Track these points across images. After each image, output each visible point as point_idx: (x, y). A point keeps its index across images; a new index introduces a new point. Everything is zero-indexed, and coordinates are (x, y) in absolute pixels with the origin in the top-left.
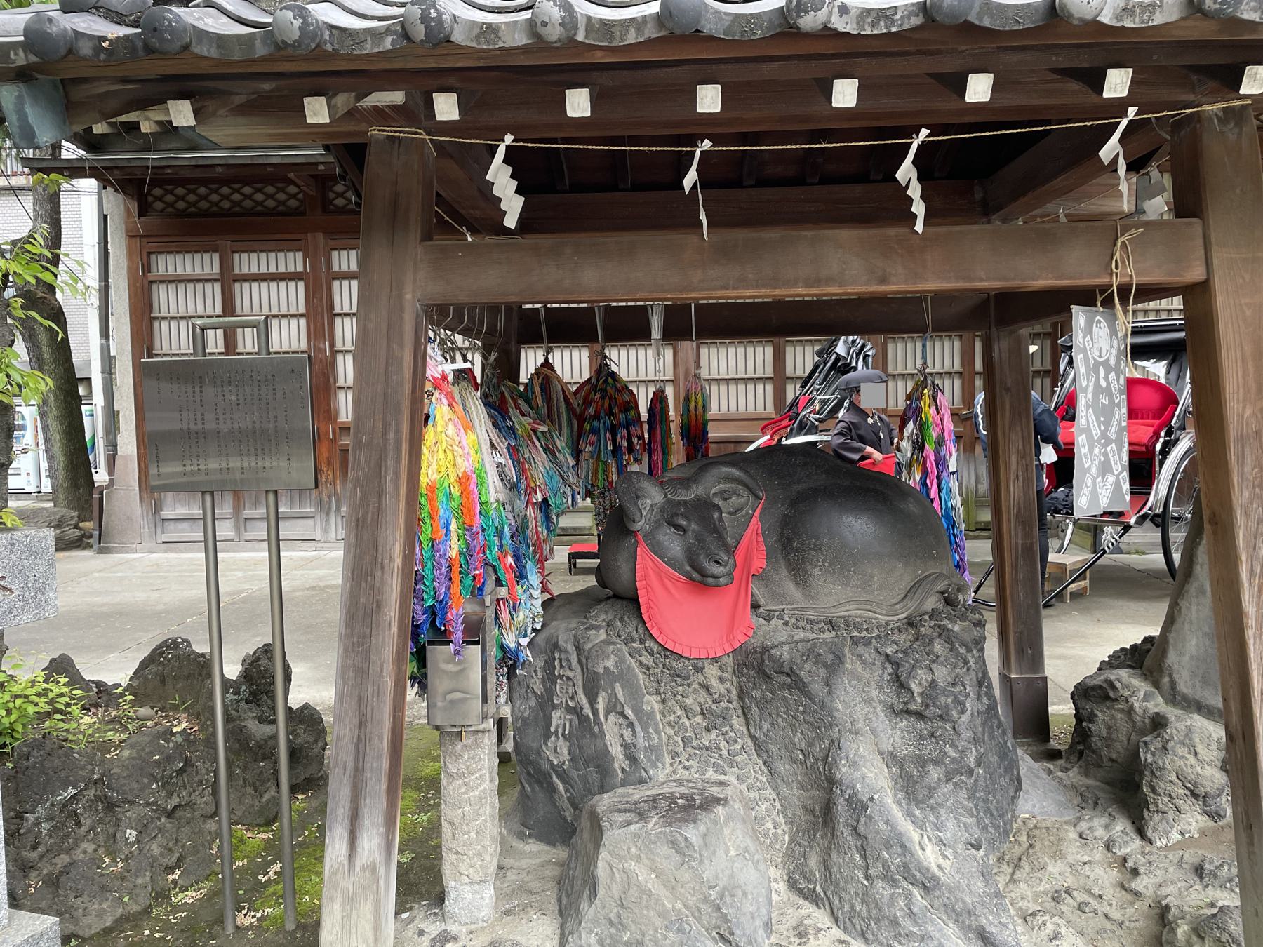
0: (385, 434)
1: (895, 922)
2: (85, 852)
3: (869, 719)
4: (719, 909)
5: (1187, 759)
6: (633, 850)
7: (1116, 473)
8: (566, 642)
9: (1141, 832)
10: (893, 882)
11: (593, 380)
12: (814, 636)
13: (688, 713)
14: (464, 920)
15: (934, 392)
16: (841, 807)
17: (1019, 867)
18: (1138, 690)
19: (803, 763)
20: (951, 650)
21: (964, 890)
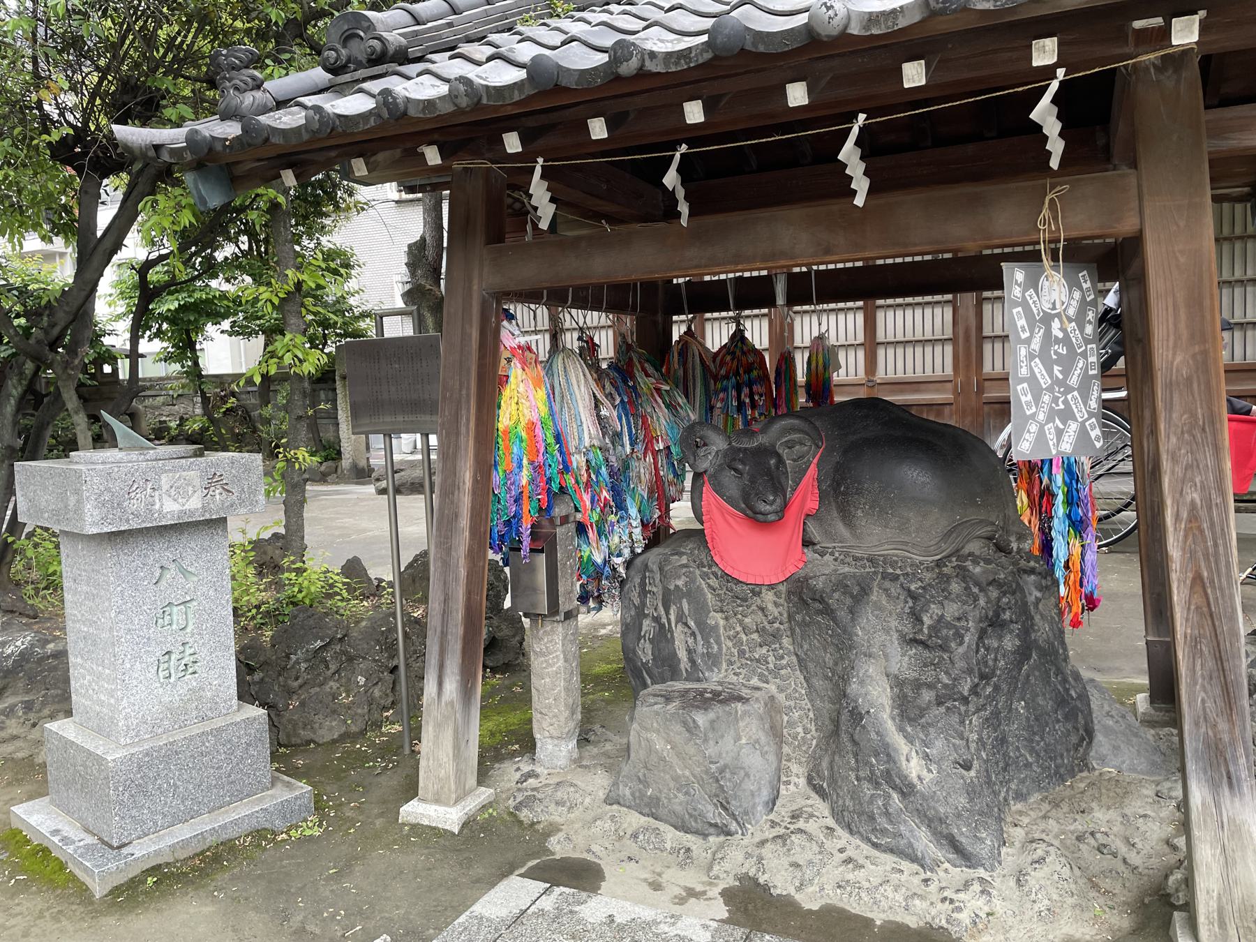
0: (460, 391)
1: (872, 818)
2: (331, 688)
4: (717, 781)
7: (1080, 420)
8: (653, 564)
10: (877, 785)
14: (547, 765)
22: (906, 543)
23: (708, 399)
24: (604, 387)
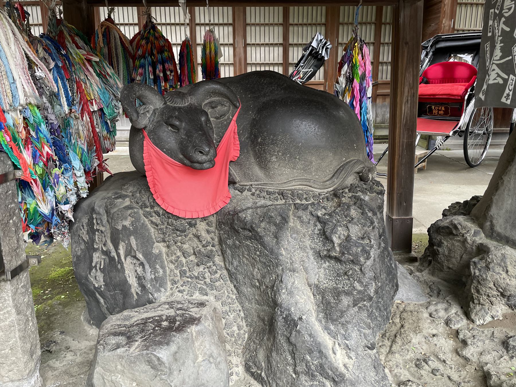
3: (303, 261)
5: (501, 274)
6: (119, 367)
8: (100, 207)
9: (467, 315)
10: (313, 377)
11: (142, 32)
12: (270, 203)
13: (185, 254)
15: (361, 45)
16: (280, 323)
17: (396, 342)
18: (470, 230)
19: (259, 288)
20: (362, 214)
21: (361, 382)
22: (309, 180)
23: (129, 74)
24: (37, 51)
